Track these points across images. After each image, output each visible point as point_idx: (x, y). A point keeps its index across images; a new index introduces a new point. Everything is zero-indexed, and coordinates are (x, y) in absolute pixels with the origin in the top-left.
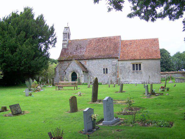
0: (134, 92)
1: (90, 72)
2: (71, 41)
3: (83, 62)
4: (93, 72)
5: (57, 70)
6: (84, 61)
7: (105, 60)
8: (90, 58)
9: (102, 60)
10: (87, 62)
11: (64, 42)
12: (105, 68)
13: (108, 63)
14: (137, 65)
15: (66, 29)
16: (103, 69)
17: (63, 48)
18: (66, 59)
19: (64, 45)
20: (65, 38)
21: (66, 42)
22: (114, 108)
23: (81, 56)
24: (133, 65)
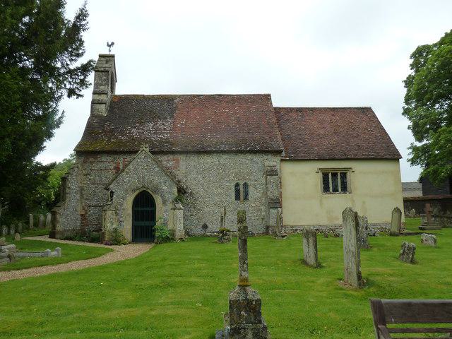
0: (14, 309)
1: (191, 194)
2: (116, 96)
3: (167, 161)
4: (202, 192)
5: (73, 185)
6: (171, 157)
7: (241, 158)
8: (189, 148)
9: (232, 156)
10: (181, 162)
11: (97, 97)
12: (241, 183)
13: (251, 166)
14: (334, 175)
15: (102, 59)
16: (233, 185)
17: (92, 115)
18: (107, 148)
19: (98, 106)
20: (101, 85)
21: (103, 97)
22: (372, 317)
23: (160, 142)
24: (325, 176)
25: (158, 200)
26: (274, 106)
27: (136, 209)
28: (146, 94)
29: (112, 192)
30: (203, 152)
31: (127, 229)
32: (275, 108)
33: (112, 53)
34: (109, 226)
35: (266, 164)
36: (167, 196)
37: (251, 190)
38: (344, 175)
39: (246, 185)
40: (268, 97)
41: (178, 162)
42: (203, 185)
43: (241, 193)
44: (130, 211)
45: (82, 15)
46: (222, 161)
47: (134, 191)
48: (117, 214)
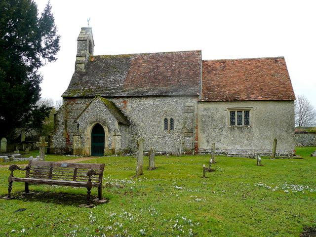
4: (142, 125)
10: (128, 104)
11: (79, 59)
12: (169, 118)
17: (76, 72)
19: (79, 65)
21: (83, 59)
24: (232, 113)
25: (106, 130)
26: (202, 59)
27: (96, 135)
28: (112, 54)
29: (78, 124)
30: (247, 101)
31: (88, 147)
32: (204, 61)
33: (90, 26)
34: (75, 146)
35: (187, 104)
36: (111, 127)
37: (175, 123)
38: (247, 113)
39: (172, 120)
40: (199, 53)
41: (126, 103)
42: (142, 119)
43: (169, 124)
44: (90, 136)
45: (48, 9)
46: (156, 103)
47: (91, 123)
48: (81, 138)
